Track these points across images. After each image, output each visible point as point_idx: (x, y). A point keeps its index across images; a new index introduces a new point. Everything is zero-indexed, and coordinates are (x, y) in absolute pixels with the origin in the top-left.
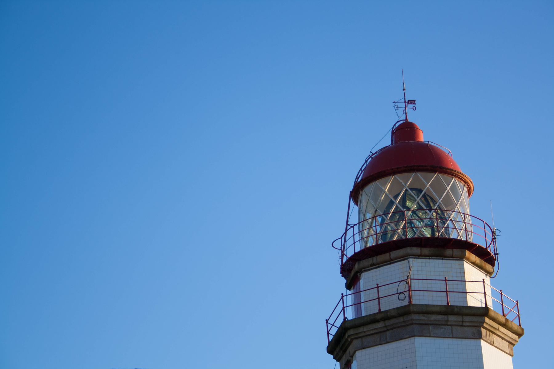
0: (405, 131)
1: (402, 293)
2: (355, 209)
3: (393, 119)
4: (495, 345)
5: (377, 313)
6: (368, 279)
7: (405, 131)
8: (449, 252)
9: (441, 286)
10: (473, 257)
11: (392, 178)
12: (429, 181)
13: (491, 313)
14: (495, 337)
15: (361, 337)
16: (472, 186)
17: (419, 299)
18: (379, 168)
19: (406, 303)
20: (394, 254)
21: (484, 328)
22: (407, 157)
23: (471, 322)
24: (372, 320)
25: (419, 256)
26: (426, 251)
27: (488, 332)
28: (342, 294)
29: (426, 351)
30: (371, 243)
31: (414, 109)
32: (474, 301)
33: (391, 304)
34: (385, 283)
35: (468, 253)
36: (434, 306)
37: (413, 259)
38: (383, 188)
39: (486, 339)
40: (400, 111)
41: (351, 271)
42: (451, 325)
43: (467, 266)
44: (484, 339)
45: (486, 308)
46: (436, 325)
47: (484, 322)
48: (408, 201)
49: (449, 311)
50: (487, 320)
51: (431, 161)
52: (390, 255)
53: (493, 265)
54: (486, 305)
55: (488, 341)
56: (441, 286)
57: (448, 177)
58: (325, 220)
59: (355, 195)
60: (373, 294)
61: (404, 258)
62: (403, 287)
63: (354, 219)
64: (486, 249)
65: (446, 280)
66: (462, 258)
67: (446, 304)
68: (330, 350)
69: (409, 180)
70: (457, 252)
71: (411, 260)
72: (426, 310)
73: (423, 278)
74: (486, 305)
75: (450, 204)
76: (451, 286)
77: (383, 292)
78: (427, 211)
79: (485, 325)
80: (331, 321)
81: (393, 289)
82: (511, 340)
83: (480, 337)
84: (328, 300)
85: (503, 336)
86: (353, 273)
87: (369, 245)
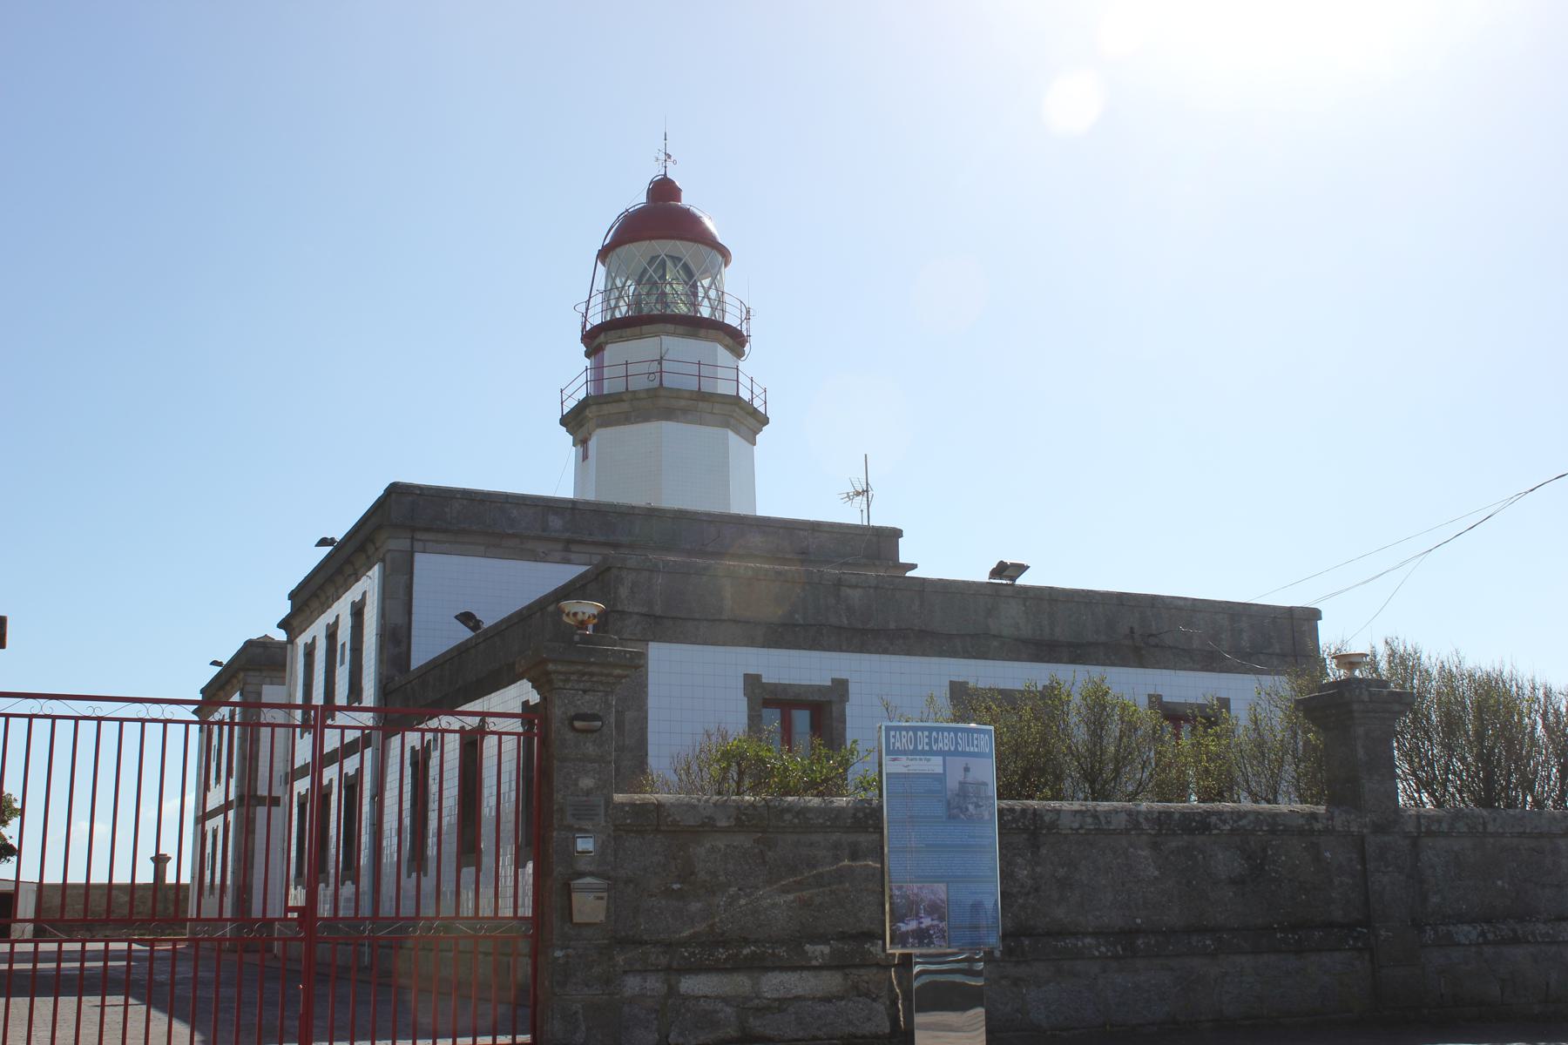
0: (663, 190)
2: (601, 269)
3: (655, 172)
6: (615, 352)
7: (663, 190)
9: (694, 369)
17: (668, 382)
19: (656, 384)
22: (660, 226)
24: (615, 398)
30: (623, 311)
31: (1021, 568)
34: (634, 356)
38: (1177, 816)
41: (594, 340)
49: (702, 396)
51: (686, 227)
56: (694, 369)
58: (576, 287)
59: (604, 254)
60: (621, 371)
62: (655, 367)
63: (600, 284)
68: (565, 421)
69: (663, 247)
72: (677, 393)
76: (705, 371)
77: (632, 369)
80: (567, 392)
81: (644, 368)
84: (571, 374)
87: (618, 315)
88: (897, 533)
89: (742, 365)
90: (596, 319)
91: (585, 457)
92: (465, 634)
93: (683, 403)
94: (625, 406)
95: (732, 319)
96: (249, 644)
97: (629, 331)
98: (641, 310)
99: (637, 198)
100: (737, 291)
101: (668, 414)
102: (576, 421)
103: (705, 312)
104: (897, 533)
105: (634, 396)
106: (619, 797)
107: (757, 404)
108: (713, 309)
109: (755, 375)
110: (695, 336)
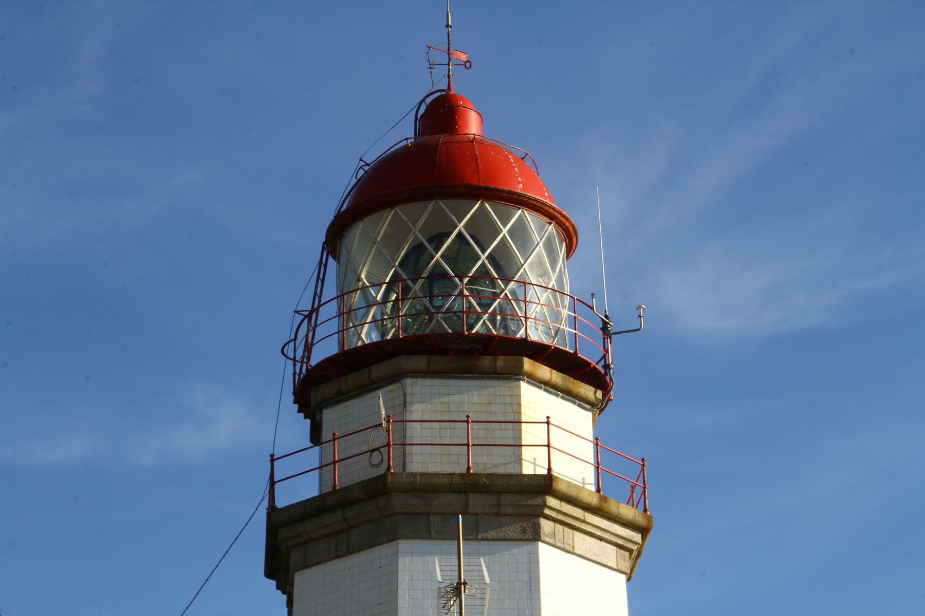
0: (441, 113)
1: (377, 449)
4: (577, 551)
5: (329, 493)
8: (486, 362)
10: (545, 372)
11: (389, 216)
13: (560, 487)
14: (578, 536)
15: (305, 543)
16: (567, 224)
20: (378, 370)
21: (548, 518)
23: (515, 506)
25: (439, 373)
26: (440, 362)
27: (559, 527)
29: (421, 569)
32: (532, 463)
35: (528, 364)
36: (436, 475)
37: (414, 380)
39: (552, 541)
40: (440, 71)
42: (476, 515)
43: (527, 391)
44: (547, 539)
47: (545, 505)
49: (469, 486)
50: (551, 501)
52: (370, 372)
54: (549, 469)
55: (558, 544)
57: (504, 208)
61: (395, 378)
64: (576, 353)
65: (548, 423)
66: (516, 374)
67: (545, 472)
70: (501, 362)
71: (408, 381)
72: (428, 486)
74: (549, 469)
75: (504, 266)
78: (409, 282)
79: (547, 511)
82: (620, 542)
83: (536, 536)
85: (599, 533)
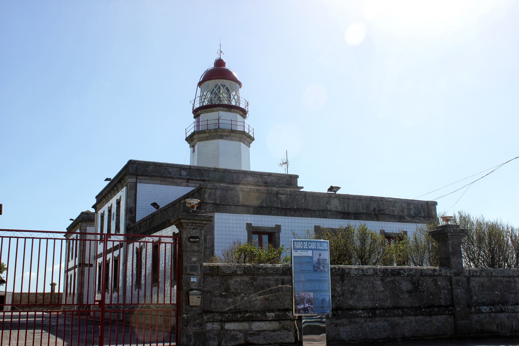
0: (220, 63)
2: (199, 89)
6: (203, 117)
7: (220, 63)
8: (233, 110)
9: (230, 122)
12: (226, 82)
18: (209, 76)
22: (219, 74)
24: (203, 132)
26: (225, 109)
28: (223, 54)
30: (206, 103)
33: (212, 127)
34: (210, 118)
38: (389, 270)
41: (197, 113)
45: (244, 132)
46: (227, 136)
48: (124, 189)
49: (232, 131)
53: (244, 117)
56: (230, 122)
58: (191, 95)
59: (200, 84)
60: (205, 123)
62: (217, 122)
63: (199, 94)
68: (187, 139)
69: (220, 82)
72: (224, 130)
73: (225, 118)
76: (233, 123)
81: (213, 122)
84: (189, 124)
86: (198, 113)
87: (204, 104)
88: (297, 177)
89: (246, 121)
90: (197, 106)
91: (194, 151)
92: (108, 182)
93: (226, 133)
94: (207, 135)
95: (242, 106)
96: (83, 213)
97: (208, 110)
98: (212, 103)
99: (211, 65)
100: (244, 96)
101: (221, 137)
102: (190, 139)
103: (233, 103)
104: (297, 177)
105: (210, 131)
106: (205, 264)
107: (251, 134)
108: (236, 102)
109: (250, 124)
110: (230, 111)
